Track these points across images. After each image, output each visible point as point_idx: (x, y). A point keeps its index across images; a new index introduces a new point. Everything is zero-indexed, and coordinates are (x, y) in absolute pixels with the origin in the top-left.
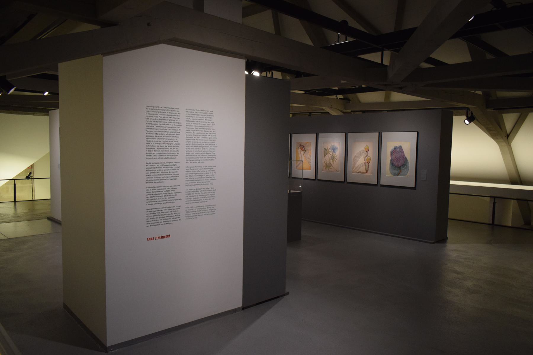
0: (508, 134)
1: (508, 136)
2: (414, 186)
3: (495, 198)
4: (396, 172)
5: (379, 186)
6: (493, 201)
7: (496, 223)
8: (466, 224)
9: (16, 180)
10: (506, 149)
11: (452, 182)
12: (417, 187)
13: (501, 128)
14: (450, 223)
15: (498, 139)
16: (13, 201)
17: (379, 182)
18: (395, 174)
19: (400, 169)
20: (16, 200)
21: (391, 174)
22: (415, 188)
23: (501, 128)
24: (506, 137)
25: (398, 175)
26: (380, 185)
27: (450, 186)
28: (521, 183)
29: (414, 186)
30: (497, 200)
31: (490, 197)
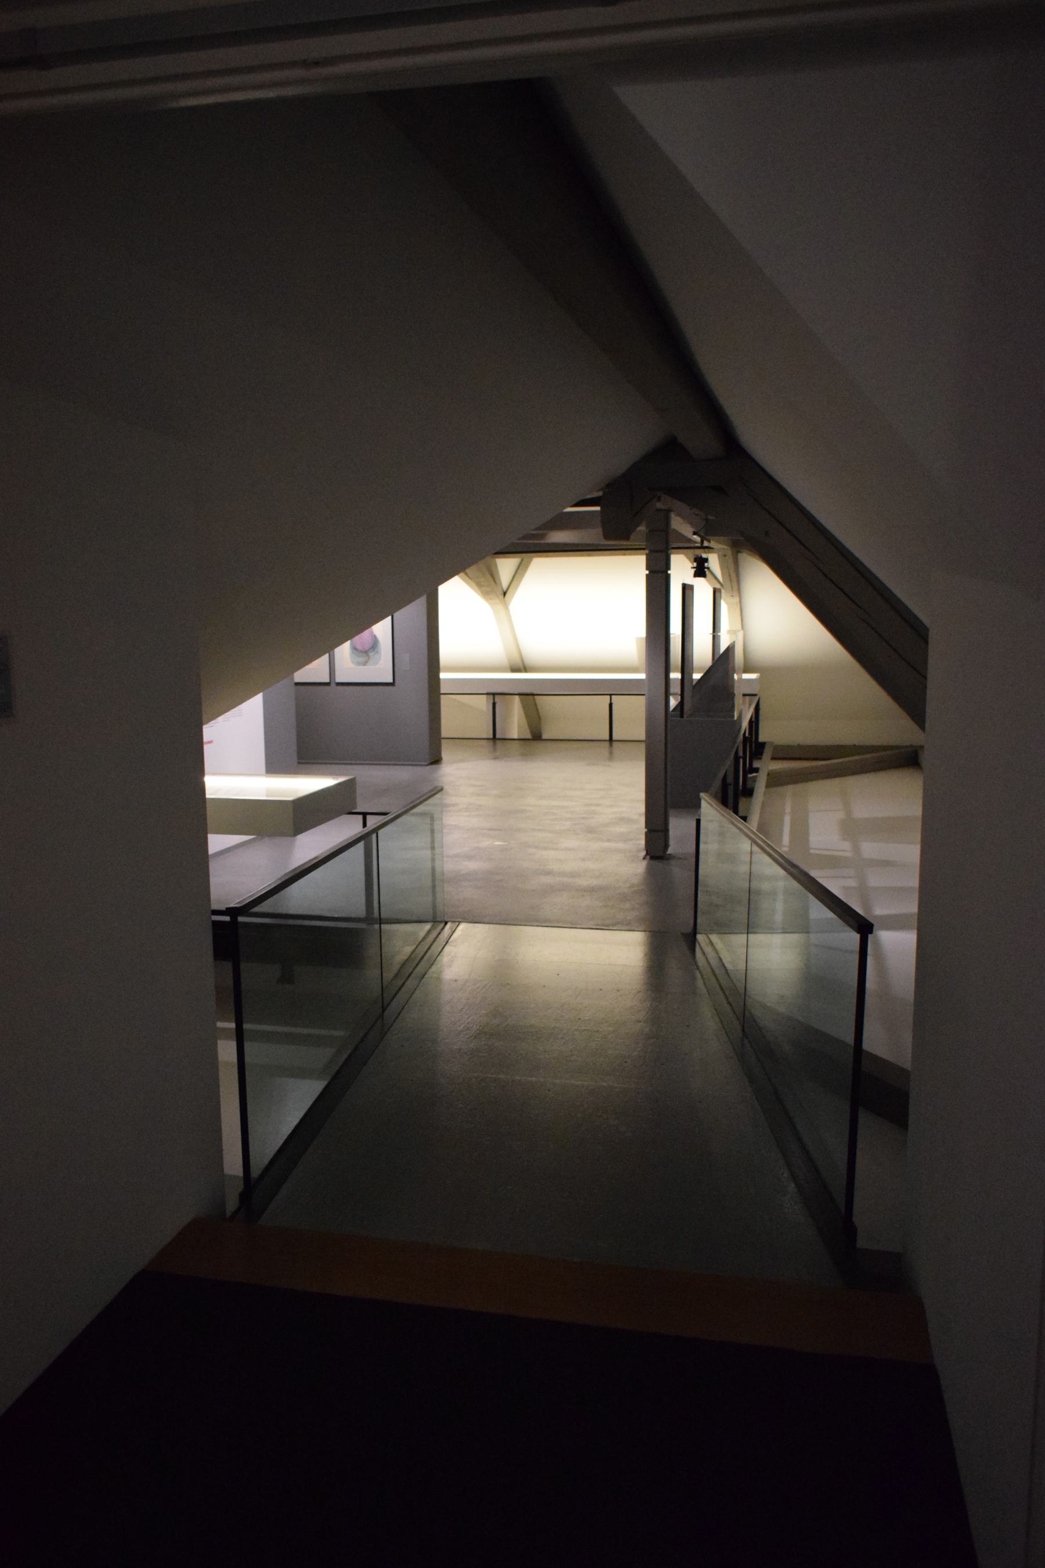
0: (505, 589)
1: (505, 594)
2: (391, 681)
3: (494, 694)
4: (362, 660)
5: (333, 685)
6: (492, 701)
7: (498, 736)
8: (463, 740)
9: (368, 817)
10: (730, 559)
11: (443, 675)
12: (396, 681)
13: (495, 582)
14: (443, 741)
15: (491, 599)
16: (607, 738)
17: (332, 679)
18: (359, 664)
19: (368, 655)
20: (615, 737)
21: (353, 662)
22: (392, 684)
23: (495, 582)
24: (502, 596)
25: (365, 664)
26: (335, 684)
27: (442, 682)
28: (525, 669)
29: (391, 681)
30: (497, 698)
31: (487, 694)
